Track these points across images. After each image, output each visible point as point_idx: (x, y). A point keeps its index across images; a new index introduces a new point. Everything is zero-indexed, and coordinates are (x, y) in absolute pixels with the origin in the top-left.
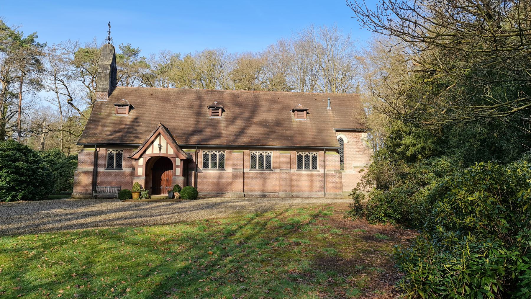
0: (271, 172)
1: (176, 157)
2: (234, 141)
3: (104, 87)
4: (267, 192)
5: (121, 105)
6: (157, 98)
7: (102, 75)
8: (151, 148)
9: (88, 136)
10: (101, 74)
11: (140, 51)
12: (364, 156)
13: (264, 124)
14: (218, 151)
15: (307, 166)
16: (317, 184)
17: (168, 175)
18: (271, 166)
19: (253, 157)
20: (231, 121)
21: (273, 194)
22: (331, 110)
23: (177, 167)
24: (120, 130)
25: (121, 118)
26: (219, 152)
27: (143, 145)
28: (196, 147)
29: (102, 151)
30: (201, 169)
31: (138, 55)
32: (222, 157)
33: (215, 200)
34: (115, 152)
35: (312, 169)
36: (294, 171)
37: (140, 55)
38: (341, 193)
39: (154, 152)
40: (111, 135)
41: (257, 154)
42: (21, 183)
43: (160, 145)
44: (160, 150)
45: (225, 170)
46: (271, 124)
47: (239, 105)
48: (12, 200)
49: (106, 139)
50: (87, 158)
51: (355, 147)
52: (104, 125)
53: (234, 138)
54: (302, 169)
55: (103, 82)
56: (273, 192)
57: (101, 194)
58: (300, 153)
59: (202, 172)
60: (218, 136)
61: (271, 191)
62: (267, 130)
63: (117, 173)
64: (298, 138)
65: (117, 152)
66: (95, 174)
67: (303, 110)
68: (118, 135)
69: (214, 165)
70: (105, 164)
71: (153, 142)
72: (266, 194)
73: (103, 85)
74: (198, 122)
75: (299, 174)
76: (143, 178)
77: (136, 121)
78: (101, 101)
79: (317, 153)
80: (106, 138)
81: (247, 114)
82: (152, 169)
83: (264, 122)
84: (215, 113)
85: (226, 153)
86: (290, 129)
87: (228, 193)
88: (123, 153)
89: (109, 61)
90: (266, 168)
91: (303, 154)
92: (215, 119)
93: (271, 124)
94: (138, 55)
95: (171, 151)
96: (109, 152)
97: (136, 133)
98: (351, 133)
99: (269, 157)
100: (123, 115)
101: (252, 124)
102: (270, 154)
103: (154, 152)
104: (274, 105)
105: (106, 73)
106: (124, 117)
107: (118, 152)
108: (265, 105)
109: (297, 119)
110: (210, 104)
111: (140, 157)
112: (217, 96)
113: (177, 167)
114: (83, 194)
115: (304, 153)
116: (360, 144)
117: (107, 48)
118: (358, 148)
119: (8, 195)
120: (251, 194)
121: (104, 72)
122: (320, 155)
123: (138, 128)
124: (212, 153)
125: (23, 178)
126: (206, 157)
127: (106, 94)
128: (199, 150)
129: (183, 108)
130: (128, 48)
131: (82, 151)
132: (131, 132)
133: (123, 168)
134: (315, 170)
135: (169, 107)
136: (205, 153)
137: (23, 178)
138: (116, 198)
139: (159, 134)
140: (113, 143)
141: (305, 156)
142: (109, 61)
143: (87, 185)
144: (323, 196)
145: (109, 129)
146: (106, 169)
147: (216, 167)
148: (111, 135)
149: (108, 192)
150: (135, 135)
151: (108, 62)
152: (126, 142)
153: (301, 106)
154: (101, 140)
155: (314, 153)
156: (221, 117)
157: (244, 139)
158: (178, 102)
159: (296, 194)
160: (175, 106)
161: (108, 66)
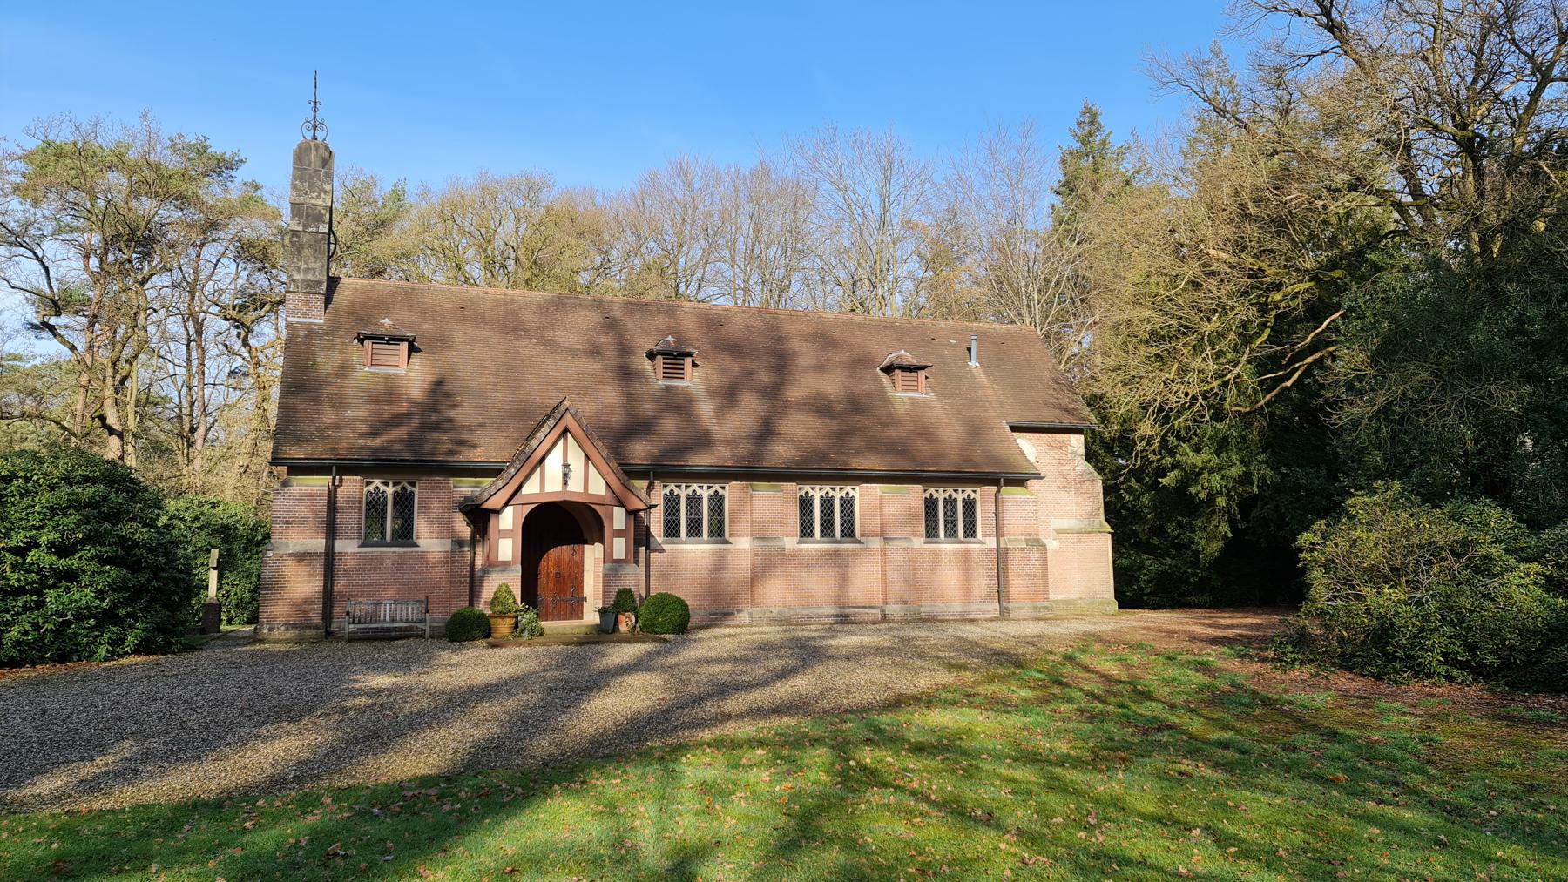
0: (858, 546)
1: (613, 502)
2: (755, 455)
3: (310, 277)
4: (849, 607)
5: (383, 339)
6: (480, 320)
7: (305, 238)
9: (298, 439)
10: (298, 236)
11: (242, 161)
12: (1081, 499)
13: (819, 407)
14: (684, 485)
15: (951, 531)
16: (983, 580)
17: (558, 563)
19: (805, 504)
20: (728, 395)
21: (866, 610)
22: (980, 370)
23: (619, 533)
24: (396, 421)
25: (387, 378)
26: (709, 488)
27: (519, 466)
28: (649, 471)
29: (351, 485)
31: (233, 174)
32: (717, 502)
33: (761, 633)
34: (390, 490)
35: (687, 535)
36: (919, 542)
37: (242, 175)
38: (1046, 604)
39: (548, 489)
40: (374, 433)
41: (817, 493)
42: (136, 593)
43: (566, 466)
44: (565, 483)
45: (727, 542)
46: (840, 408)
47: (734, 348)
48: (112, 655)
49: (362, 448)
50: (304, 510)
51: (1057, 475)
52: (340, 402)
53: (749, 445)
54: (938, 536)
55: (306, 263)
56: (864, 607)
57: (362, 626)
58: (932, 490)
59: (662, 551)
60: (703, 440)
61: (859, 604)
62: (833, 425)
63: (400, 555)
64: (924, 448)
65: (398, 488)
66: (330, 561)
67: (917, 369)
68: (400, 433)
69: (695, 529)
70: (359, 529)
72: (848, 611)
73: (307, 270)
74: (630, 398)
75: (933, 551)
76: (517, 571)
77: (438, 387)
78: (305, 323)
79: (723, 488)
80: (362, 442)
81: (764, 377)
83: (815, 399)
84: (674, 371)
85: (731, 492)
86: (891, 422)
87: (739, 611)
88: (416, 491)
89: (323, 195)
90: (842, 536)
91: (940, 494)
92: (677, 387)
93: (840, 408)
94: (233, 174)
95: (598, 487)
96: (371, 488)
97: (454, 429)
98: (1044, 435)
99: (848, 504)
100: (392, 371)
101: (787, 405)
102: (852, 493)
103: (548, 489)
104: (828, 352)
105: (317, 232)
106: (396, 376)
107: (399, 490)
108: (805, 354)
109: (903, 395)
110: (649, 344)
111: (506, 504)
112: (660, 321)
114: (294, 626)
115: (941, 490)
116: (1068, 467)
117: (313, 152)
118: (1064, 478)
119: (97, 637)
120: (805, 612)
121: (311, 230)
122: (983, 496)
123: (452, 413)
124: (690, 491)
125: (141, 579)
126: (671, 503)
127: (319, 300)
128: (341, 479)
129: (572, 352)
130: (202, 150)
131: (285, 484)
132: (436, 427)
133: (421, 542)
134: (972, 539)
135: (526, 348)
136: (667, 491)
137: (141, 579)
138: (423, 636)
139: (566, 431)
140: (390, 460)
141: (688, 498)
142: (323, 195)
143: (307, 601)
144: (997, 614)
145: (358, 415)
146: (362, 545)
147: (811, 534)
148: (374, 433)
149: (388, 619)
150: (452, 435)
151: (318, 197)
152: (433, 455)
153: (908, 358)
154: (349, 450)
155: (969, 491)
156: (693, 380)
157: (780, 452)
158: (549, 335)
159: (927, 609)
160: (545, 346)
161: (323, 211)
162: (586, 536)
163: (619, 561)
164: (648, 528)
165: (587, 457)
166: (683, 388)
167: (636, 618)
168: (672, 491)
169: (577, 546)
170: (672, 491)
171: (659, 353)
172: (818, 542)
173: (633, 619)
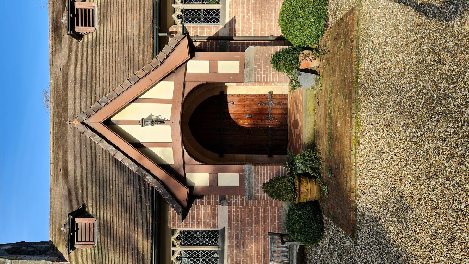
8: (156, 151)
18: (210, 231)
30: (221, 26)
43: (143, 123)
44: (162, 122)
45: (223, 230)
54: (218, 10)
59: (233, 21)
71: (138, 145)
82: (221, 156)
107: (179, 242)
113: (214, 67)
134: (221, 15)
139: (108, 123)
149: (288, 254)
162: (217, 93)
163: (242, 67)
164: (210, 38)
165: (134, 100)
166: (99, 9)
167: (304, 48)
168: (179, 17)
169: (229, 100)
170: (179, 17)
171: (72, 28)
172: (224, 5)
173: (306, 52)
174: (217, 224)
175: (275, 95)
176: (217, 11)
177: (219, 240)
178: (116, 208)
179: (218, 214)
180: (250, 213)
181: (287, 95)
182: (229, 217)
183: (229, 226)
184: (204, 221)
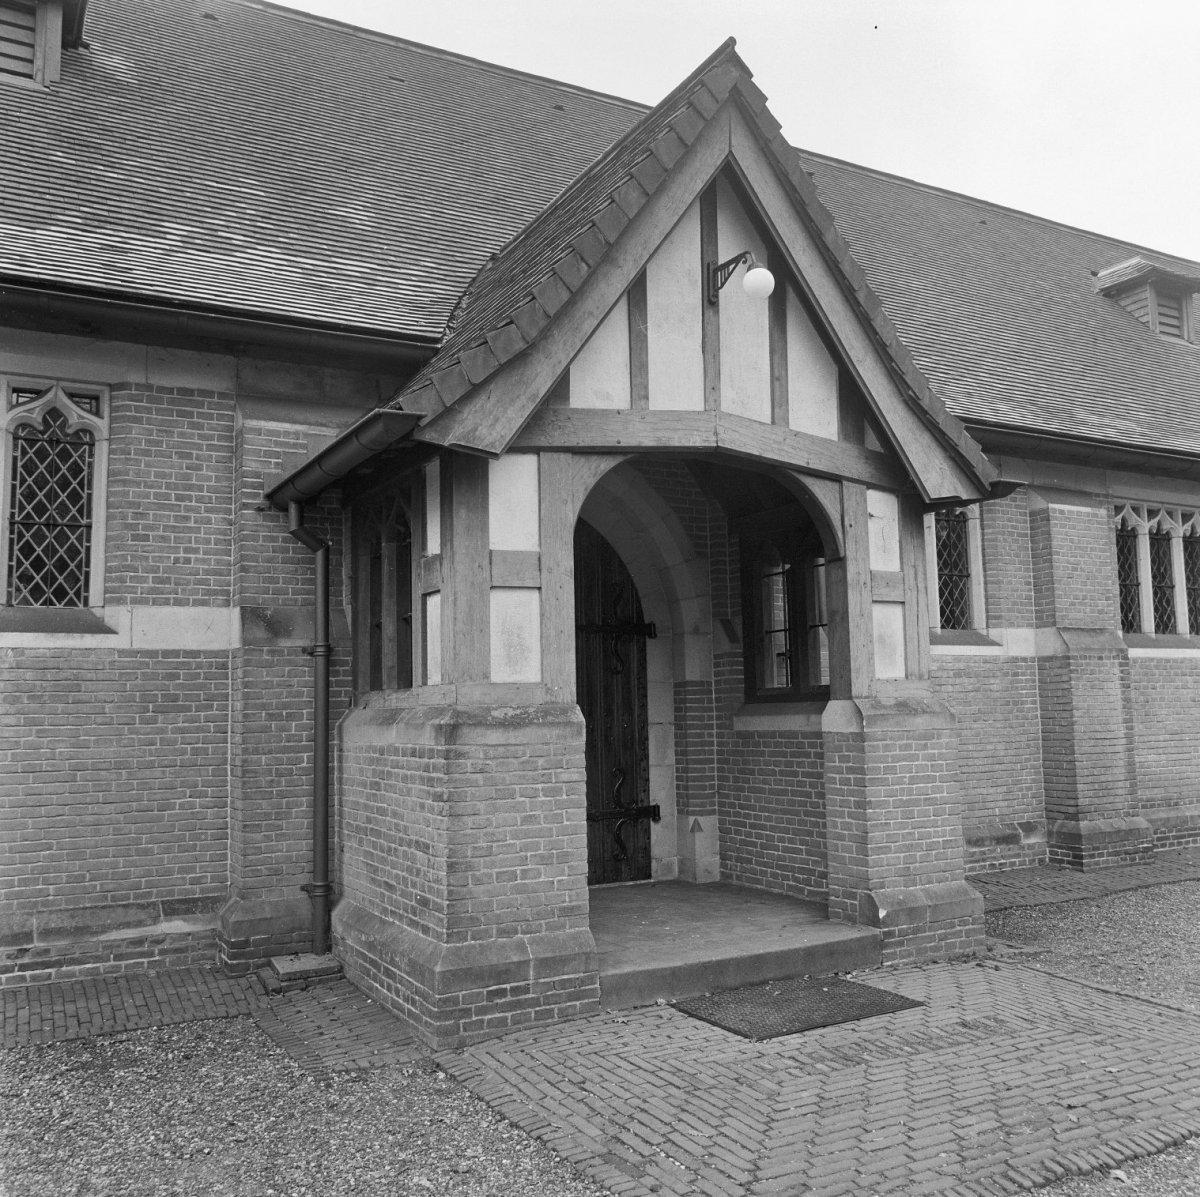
54: (1174, 630)
107: (36, 418)
174: (135, 601)
175: (647, 832)
176: (78, 594)
177: (37, 606)
178: (336, 228)
179: (178, 603)
180: (183, 752)
181: (649, 876)
182: (167, 653)
183: (122, 652)
184: (146, 538)
